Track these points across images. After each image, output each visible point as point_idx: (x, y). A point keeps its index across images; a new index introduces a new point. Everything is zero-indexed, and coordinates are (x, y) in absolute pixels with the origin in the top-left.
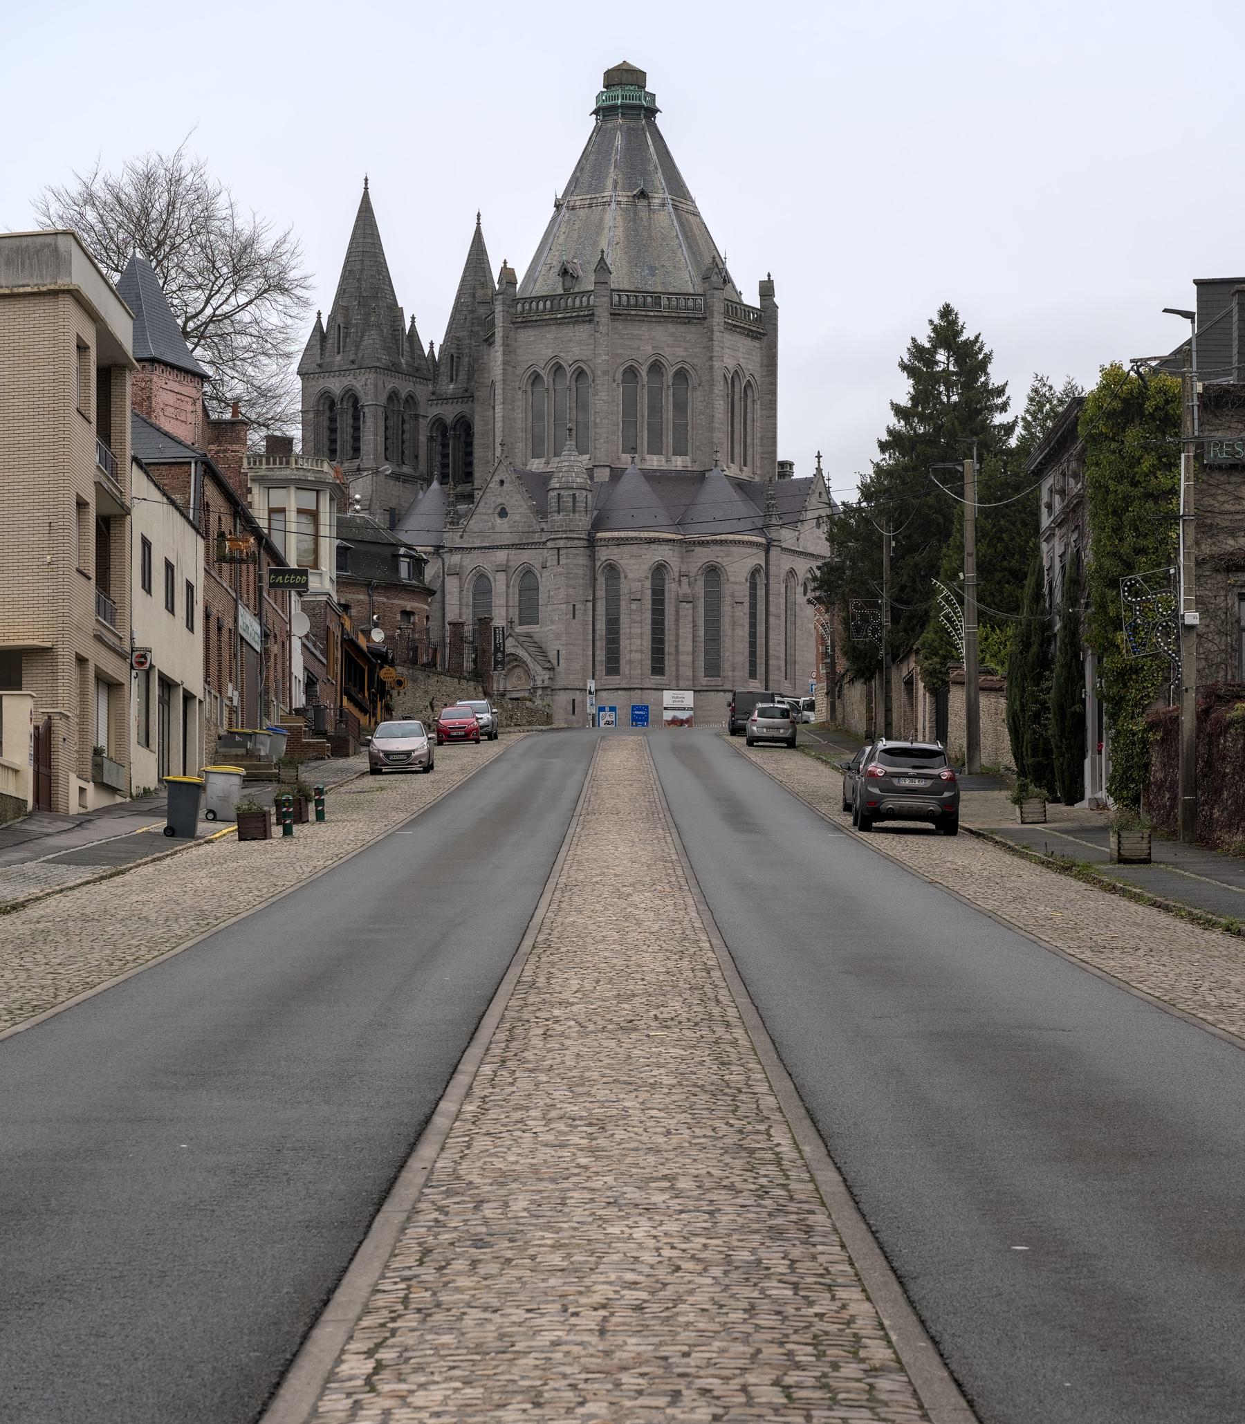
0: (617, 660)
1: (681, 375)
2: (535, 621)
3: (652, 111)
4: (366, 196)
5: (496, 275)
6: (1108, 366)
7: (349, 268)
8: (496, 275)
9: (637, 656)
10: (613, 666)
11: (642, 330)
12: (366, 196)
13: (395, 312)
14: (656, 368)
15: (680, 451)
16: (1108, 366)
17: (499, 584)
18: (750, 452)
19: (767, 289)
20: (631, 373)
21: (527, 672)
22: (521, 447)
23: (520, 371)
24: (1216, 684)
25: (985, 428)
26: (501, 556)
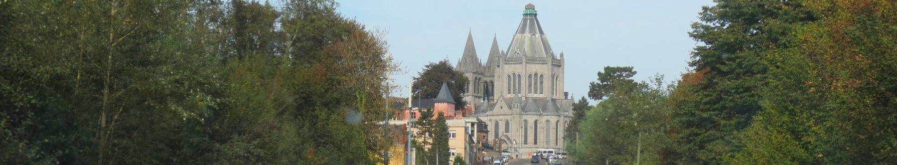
0: (527, 141)
1: (542, 76)
2: (508, 132)
3: (536, 15)
4: (495, 38)
5: (500, 52)
6: (603, 71)
7: (492, 53)
8: (500, 52)
9: (531, 141)
10: (526, 143)
11: (533, 66)
12: (495, 38)
13: (477, 59)
14: (536, 74)
15: (541, 93)
16: (603, 71)
17: (500, 123)
18: (557, 92)
19: (562, 55)
20: (530, 76)
21: (507, 143)
22: (506, 91)
23: (505, 74)
24: (696, 128)
25: (60, 76)
26: (501, 117)
